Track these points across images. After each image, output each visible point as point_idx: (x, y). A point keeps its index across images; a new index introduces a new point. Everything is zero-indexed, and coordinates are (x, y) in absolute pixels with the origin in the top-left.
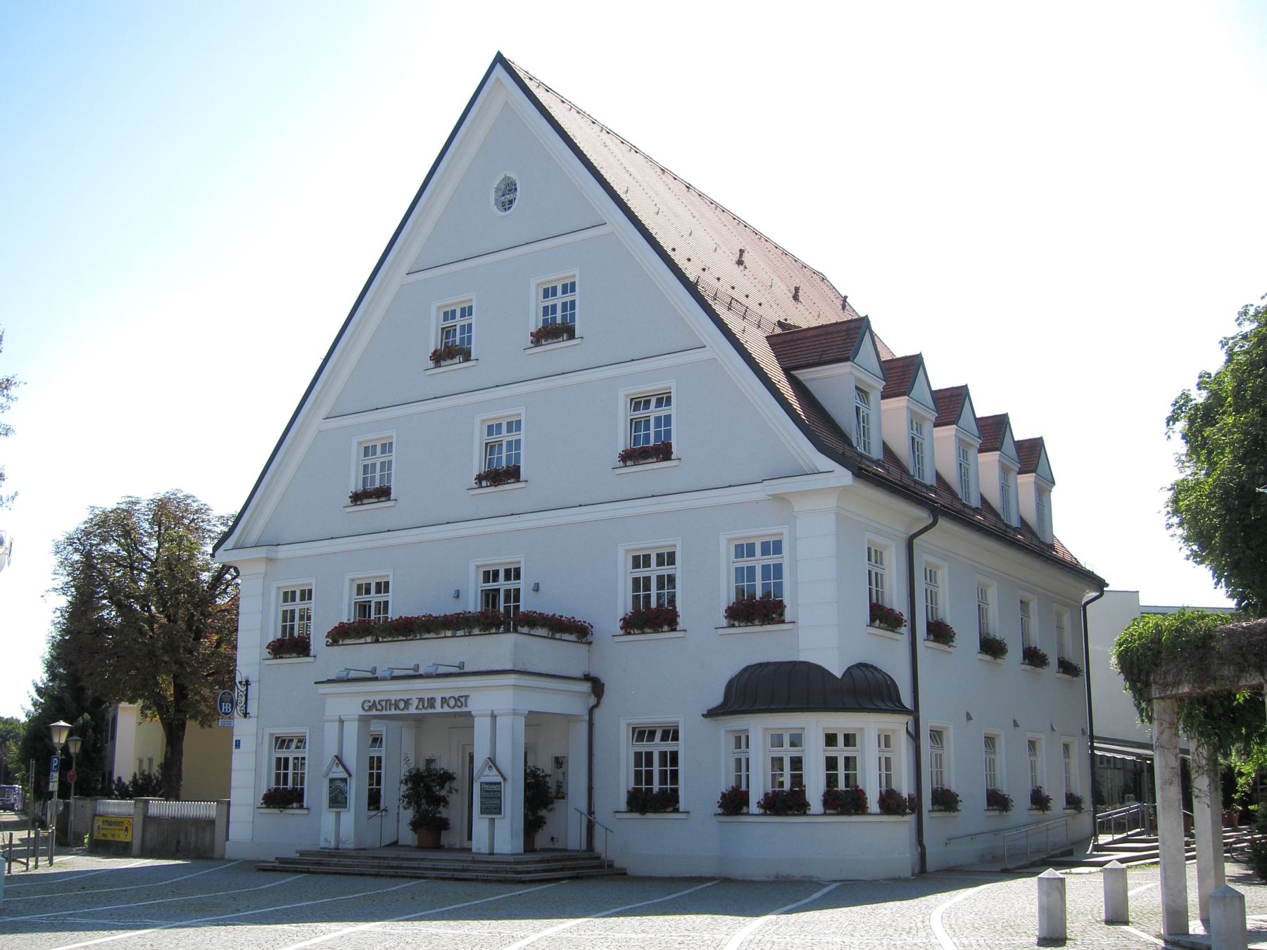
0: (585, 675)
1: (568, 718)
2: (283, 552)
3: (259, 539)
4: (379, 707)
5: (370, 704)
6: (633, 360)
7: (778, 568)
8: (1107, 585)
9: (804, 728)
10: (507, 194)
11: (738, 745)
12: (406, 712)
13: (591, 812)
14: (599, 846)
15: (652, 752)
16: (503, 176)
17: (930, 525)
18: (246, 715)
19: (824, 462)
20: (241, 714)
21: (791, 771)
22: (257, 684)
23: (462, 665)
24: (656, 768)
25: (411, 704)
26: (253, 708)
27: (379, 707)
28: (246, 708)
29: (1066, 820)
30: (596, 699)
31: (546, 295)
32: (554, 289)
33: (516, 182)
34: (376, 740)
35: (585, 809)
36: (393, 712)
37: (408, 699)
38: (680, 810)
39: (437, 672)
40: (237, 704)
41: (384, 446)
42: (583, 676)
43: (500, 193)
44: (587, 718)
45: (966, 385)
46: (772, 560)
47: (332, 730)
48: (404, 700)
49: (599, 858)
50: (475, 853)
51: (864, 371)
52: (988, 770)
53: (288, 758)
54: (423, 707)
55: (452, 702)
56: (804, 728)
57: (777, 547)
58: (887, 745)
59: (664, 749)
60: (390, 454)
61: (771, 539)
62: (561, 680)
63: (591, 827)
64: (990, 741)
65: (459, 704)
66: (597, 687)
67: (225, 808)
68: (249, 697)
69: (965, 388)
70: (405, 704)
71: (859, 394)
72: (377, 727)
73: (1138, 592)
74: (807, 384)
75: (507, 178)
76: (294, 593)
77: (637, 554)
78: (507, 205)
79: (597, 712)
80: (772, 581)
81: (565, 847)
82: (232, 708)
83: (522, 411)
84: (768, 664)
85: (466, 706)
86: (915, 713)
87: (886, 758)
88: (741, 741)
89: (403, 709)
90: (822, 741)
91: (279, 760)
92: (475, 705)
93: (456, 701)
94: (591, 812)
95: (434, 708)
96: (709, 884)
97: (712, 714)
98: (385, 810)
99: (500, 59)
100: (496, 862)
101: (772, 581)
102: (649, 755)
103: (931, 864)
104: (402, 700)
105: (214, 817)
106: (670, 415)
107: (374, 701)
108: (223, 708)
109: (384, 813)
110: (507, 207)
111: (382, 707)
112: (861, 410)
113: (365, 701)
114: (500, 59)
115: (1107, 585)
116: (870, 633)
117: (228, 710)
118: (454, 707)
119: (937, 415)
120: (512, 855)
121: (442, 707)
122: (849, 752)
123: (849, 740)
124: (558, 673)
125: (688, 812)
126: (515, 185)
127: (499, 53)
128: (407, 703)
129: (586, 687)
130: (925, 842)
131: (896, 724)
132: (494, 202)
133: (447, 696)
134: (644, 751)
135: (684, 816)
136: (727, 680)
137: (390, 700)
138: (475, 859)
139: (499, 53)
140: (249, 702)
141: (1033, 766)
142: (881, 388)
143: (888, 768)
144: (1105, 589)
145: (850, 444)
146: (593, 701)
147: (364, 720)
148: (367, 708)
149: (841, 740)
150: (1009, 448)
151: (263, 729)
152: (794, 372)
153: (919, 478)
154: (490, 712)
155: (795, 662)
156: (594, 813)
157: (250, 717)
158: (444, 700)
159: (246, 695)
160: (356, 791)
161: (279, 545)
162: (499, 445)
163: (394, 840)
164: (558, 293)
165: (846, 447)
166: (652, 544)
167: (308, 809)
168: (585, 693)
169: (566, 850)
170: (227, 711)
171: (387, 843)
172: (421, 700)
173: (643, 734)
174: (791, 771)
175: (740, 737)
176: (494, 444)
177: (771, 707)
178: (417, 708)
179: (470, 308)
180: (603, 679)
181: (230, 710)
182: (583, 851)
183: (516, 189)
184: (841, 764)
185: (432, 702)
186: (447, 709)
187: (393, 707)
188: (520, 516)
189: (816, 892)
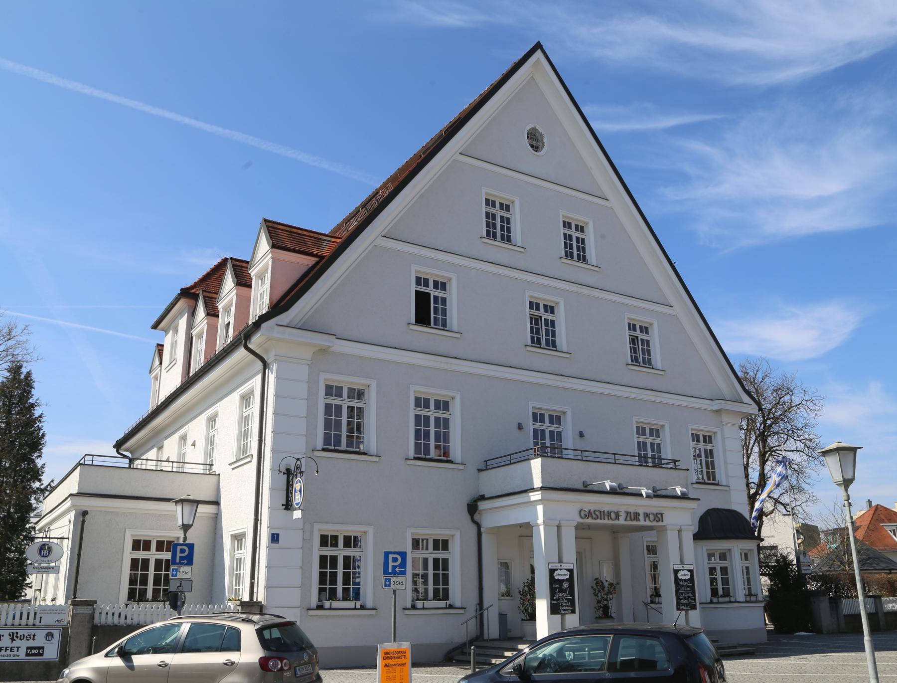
4: (594, 516)
12: (616, 522)
16: (533, 127)
21: (448, 573)
24: (151, 572)
27: (594, 516)
55: (652, 517)
58: (746, 559)
65: (657, 519)
87: (746, 567)
100: (746, 644)
101: (333, 418)
102: (334, 559)
114: (538, 46)
127: (539, 41)
133: (648, 512)
134: (441, 557)
139: (539, 41)
143: (748, 573)
149: (154, 546)
152: (316, 259)
158: (647, 515)
160: (703, 591)
167: (373, 609)
174: (448, 573)
185: (636, 516)
186: (648, 523)
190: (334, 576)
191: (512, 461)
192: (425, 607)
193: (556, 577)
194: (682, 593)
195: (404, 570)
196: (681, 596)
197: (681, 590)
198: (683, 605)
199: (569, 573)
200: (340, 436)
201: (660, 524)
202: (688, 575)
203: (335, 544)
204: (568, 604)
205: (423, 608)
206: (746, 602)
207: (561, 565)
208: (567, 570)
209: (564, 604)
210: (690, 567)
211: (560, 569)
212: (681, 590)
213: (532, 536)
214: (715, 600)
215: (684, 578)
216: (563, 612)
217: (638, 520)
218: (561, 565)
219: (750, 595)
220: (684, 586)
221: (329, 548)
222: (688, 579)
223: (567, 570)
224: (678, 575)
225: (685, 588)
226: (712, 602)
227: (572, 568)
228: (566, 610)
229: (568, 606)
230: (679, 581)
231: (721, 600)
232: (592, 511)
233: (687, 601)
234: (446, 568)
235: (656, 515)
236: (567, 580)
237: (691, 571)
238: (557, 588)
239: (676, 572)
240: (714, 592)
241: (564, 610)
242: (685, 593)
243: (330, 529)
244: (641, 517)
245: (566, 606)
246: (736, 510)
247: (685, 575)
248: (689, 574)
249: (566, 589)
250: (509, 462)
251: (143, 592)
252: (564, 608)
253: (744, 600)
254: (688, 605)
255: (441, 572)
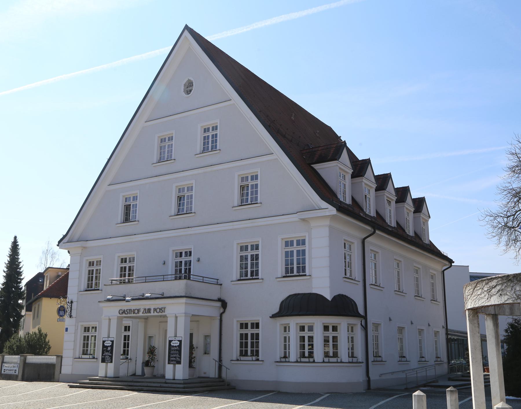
0: (218, 299)
1: (211, 318)
2: (90, 244)
3: (79, 238)
4: (126, 313)
5: (123, 311)
6: (242, 160)
7: (304, 251)
8: (454, 262)
9: (314, 323)
10: (189, 87)
11: (285, 331)
12: (138, 315)
13: (220, 360)
14: (224, 375)
15: (248, 334)
16: (187, 79)
17: (372, 233)
18: (71, 316)
19: (324, 204)
20: (69, 316)
22: (76, 303)
23: (163, 294)
24: (249, 341)
25: (140, 311)
26: (74, 314)
27: (126, 313)
28: (71, 313)
29: (435, 366)
30: (223, 309)
31: (205, 131)
32: (209, 128)
33: (193, 82)
34: (127, 328)
35: (217, 359)
36: (132, 315)
37: (139, 309)
38: (260, 360)
39: (151, 297)
40: (66, 312)
41: (134, 197)
42: (218, 299)
43: (186, 86)
44: (219, 318)
45: (409, 186)
46: (301, 248)
47: (105, 323)
48: (137, 309)
49: (223, 381)
50: (167, 379)
51: (347, 167)
52: (374, 341)
53: (89, 336)
54: (146, 313)
55: (158, 310)
56: (314, 323)
57: (303, 242)
59: (253, 332)
60: (136, 201)
61: (301, 239)
62: (207, 301)
63: (220, 367)
64: (401, 330)
65: (161, 311)
66: (224, 304)
67: (60, 358)
68: (72, 309)
69: (408, 187)
70: (138, 312)
71: (388, 202)
72: (127, 322)
73: (469, 266)
74: (318, 171)
75: (189, 80)
76: (93, 262)
77: (242, 245)
78: (188, 92)
79: (224, 316)
80: (301, 257)
81: (209, 376)
82: (64, 313)
83: (193, 182)
84: (299, 294)
85: (164, 312)
86: (365, 317)
88: (286, 329)
89: (137, 314)
90: (322, 328)
91: (85, 337)
92: (168, 312)
93: (160, 310)
94: (220, 360)
95: (150, 313)
96: (271, 394)
97: (274, 316)
98: (130, 359)
99: (187, 27)
102: (247, 335)
103: (373, 386)
104: (158, 308)
105: (55, 363)
106: (258, 184)
107: (124, 310)
108: (60, 313)
109: (129, 361)
110: (189, 93)
111: (128, 312)
112: (367, 196)
113: (120, 310)
115: (454, 262)
116: (344, 281)
117: (63, 314)
118: (159, 313)
119: (353, 171)
120: (183, 380)
121: (154, 313)
122: (335, 334)
123: (335, 329)
124: (204, 298)
125: (263, 361)
126: (193, 83)
127: (186, 25)
128: (139, 311)
129: (219, 304)
130: (370, 375)
131: (356, 322)
132: (183, 90)
135: (261, 362)
136: (281, 300)
137: (131, 310)
138: (166, 382)
139: (186, 25)
140: (72, 310)
141: (401, 340)
142: (375, 187)
143: (352, 341)
144: (453, 264)
145: (362, 210)
146: (222, 310)
147: (120, 319)
148: (121, 313)
149: (331, 328)
150: (409, 201)
151: (78, 323)
153: (344, 200)
154: (174, 315)
155: (311, 293)
156: (222, 361)
157: (72, 318)
158: (155, 310)
159: (71, 308)
161: (87, 241)
162: (183, 197)
163: (134, 373)
164: (210, 130)
165: (420, 241)
166: (248, 241)
168: (218, 307)
169: (209, 378)
170: (62, 315)
171: (130, 375)
172: (145, 309)
173: (244, 326)
175: (286, 327)
176: (181, 196)
177: (300, 313)
178: (143, 313)
179: (172, 137)
180: (227, 300)
181: (63, 314)
182: (216, 378)
183: (193, 85)
184: (377, 344)
185: (149, 311)
186: (156, 314)
187: (132, 313)
188: (192, 228)
189: (318, 398)
190: (246, 343)
191: (165, 280)
192: (330, 361)
193: (105, 345)
194: (172, 354)
195: (466, 339)
196: (172, 356)
197: (172, 352)
198: (172, 361)
199: (111, 342)
200: (247, 263)
201: (163, 314)
202: (178, 343)
203: (246, 327)
204: (109, 358)
205: (329, 362)
206: (349, 362)
207: (175, 338)
208: (111, 341)
209: (107, 358)
210: (179, 339)
211: (175, 340)
212: (172, 352)
213: (167, 322)
214: (326, 360)
215: (175, 345)
216: (106, 362)
217: (150, 312)
218: (175, 338)
219: (285, 357)
220: (174, 350)
221: (255, 329)
222: (178, 346)
223: (111, 341)
224: (171, 343)
225: (174, 351)
226: (324, 362)
227: (181, 339)
228: (108, 361)
229: (109, 359)
230: (171, 347)
231: (332, 360)
232: (125, 310)
233: (175, 359)
234: (257, 338)
235: (160, 309)
236: (110, 346)
237: (180, 341)
238: (105, 350)
239: (170, 341)
240: (303, 355)
241: (107, 361)
242: (174, 354)
243: (87, 324)
244: (152, 311)
245: (108, 359)
246: (323, 295)
247: (175, 343)
248: (111, 342)
249: (109, 350)
250: (162, 280)
251: (246, 351)
252: (107, 360)
253: (348, 361)
254: (175, 361)
255: (244, 341)
